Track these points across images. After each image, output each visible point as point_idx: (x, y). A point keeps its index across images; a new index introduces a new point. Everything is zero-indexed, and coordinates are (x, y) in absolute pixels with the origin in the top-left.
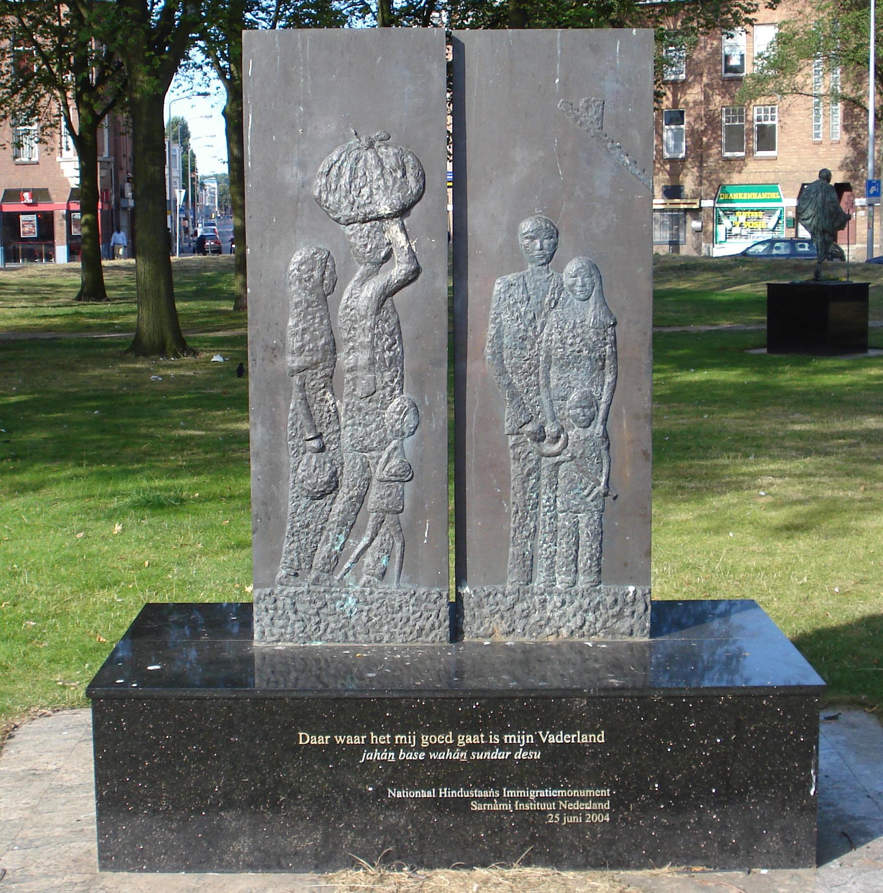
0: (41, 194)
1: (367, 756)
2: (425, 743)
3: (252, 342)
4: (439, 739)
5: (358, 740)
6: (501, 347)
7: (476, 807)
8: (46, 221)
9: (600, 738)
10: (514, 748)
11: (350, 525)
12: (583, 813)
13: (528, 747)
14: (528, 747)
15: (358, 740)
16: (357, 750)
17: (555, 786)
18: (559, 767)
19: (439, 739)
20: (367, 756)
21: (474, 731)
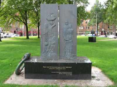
0: (36, 31)
1: (49, 69)
2: (55, 67)
3: (59, 51)
4: (56, 67)
5: (49, 67)
6: (24, 49)
7: (60, 74)
8: (36, 33)
9: (71, 67)
10: (63, 68)
11: (49, 48)
12: (70, 74)
13: (64, 68)
14: (64, 68)
15: (49, 67)
16: (49, 68)
17: (67, 72)
18: (67, 70)
19: (56, 67)
20: (49, 69)
21: (61, 72)
